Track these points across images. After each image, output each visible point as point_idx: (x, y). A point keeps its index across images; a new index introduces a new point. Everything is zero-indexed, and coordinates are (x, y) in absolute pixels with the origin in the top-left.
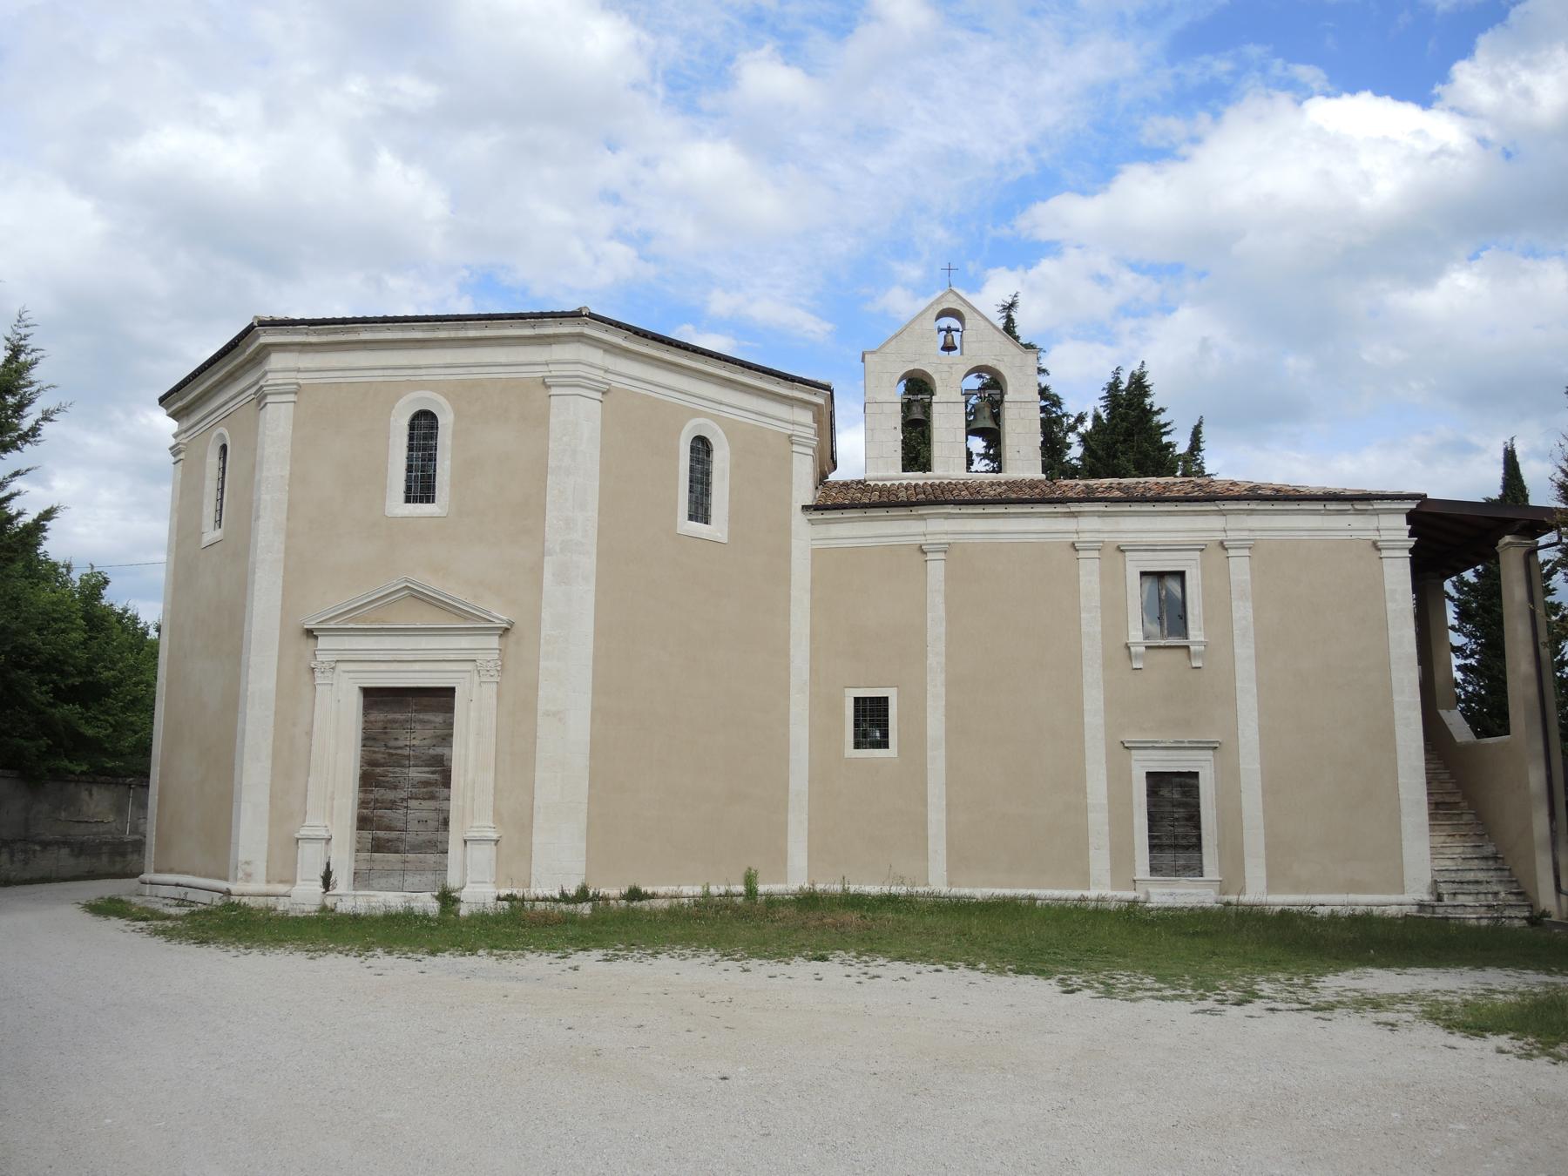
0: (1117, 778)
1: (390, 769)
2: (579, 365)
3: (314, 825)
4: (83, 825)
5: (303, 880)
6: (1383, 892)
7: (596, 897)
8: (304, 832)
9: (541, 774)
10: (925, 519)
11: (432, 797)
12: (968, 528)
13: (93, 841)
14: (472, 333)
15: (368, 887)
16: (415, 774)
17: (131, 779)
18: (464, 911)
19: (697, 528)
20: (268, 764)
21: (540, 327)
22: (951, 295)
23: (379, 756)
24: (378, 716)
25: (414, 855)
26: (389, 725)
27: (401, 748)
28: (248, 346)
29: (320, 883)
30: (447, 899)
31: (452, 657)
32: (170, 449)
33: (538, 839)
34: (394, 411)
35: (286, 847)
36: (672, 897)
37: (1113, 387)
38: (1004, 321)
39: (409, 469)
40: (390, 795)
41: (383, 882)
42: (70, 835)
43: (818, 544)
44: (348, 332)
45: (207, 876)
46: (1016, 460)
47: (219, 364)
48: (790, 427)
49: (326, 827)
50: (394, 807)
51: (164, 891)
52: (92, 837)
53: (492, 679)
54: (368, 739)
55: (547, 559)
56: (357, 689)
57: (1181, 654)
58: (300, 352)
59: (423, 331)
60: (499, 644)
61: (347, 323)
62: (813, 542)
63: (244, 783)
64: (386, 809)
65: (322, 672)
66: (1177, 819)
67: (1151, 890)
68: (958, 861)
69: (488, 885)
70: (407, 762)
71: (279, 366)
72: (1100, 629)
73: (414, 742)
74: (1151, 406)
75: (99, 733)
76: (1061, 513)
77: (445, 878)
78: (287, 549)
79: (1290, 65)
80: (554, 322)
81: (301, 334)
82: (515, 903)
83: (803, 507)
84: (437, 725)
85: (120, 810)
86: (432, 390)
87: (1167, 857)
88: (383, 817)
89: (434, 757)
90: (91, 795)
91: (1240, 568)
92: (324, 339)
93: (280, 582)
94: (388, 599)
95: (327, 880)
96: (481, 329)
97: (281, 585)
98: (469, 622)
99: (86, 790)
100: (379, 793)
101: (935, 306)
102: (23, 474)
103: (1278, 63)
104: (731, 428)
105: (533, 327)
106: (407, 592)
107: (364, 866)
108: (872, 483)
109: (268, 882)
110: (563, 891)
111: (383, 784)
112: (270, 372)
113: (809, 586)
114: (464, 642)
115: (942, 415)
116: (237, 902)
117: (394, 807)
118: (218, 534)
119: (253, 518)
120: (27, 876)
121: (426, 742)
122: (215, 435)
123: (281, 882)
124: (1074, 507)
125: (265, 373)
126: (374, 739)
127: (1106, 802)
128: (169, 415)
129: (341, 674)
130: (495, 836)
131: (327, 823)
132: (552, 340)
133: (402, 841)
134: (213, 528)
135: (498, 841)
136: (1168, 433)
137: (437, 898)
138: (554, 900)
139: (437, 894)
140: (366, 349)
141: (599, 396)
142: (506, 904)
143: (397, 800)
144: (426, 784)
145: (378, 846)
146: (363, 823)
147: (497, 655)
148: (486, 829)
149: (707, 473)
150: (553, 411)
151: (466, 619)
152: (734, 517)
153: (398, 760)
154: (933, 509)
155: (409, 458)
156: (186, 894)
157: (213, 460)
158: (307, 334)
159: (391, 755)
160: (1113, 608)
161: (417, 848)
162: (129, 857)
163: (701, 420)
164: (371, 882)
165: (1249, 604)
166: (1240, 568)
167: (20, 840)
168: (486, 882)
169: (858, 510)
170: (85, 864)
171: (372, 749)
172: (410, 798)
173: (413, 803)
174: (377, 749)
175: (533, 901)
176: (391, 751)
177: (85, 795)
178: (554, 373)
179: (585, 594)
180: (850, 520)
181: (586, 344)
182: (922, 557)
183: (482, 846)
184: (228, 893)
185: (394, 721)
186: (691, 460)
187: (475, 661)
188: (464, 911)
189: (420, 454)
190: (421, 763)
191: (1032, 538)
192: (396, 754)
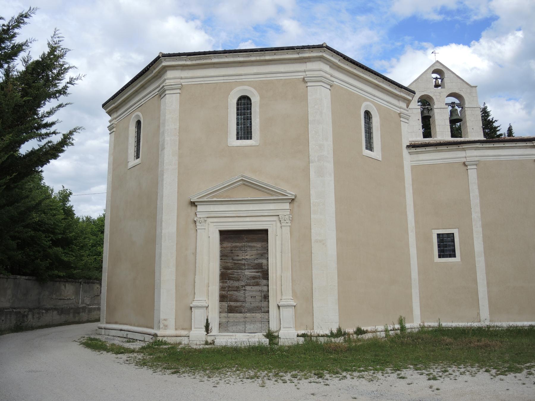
2: (321, 72)
3: (200, 299)
4: (62, 301)
7: (345, 334)
8: (194, 304)
10: (465, 150)
11: (258, 284)
13: (67, 307)
15: (227, 331)
16: (248, 273)
17: (81, 280)
20: (174, 269)
23: (229, 264)
24: (228, 245)
26: (233, 249)
28: (155, 69)
31: (266, 214)
32: (108, 127)
33: (316, 305)
34: (230, 96)
39: (238, 124)
40: (236, 284)
41: (234, 328)
42: (57, 305)
43: (414, 163)
44: (206, 59)
45: (139, 326)
46: (472, 132)
49: (205, 301)
50: (238, 290)
51: (113, 333)
52: (66, 306)
54: (223, 256)
55: (311, 164)
56: (218, 230)
58: (182, 70)
59: (243, 57)
60: (290, 207)
61: (206, 54)
62: (412, 163)
64: (234, 291)
65: (200, 223)
69: (292, 329)
70: (244, 267)
73: (247, 257)
74: (492, 119)
75: (69, 259)
76: (529, 146)
78: (179, 163)
79: (420, 43)
81: (183, 60)
84: (258, 248)
85: (77, 293)
86: (248, 86)
88: (233, 295)
90: (65, 287)
92: (194, 62)
94: (232, 186)
95: (207, 328)
96: (272, 55)
97: (177, 180)
99: (63, 285)
100: (230, 283)
101: (431, 68)
102: (63, 106)
103: (416, 42)
104: (379, 107)
106: (241, 182)
107: (224, 320)
109: (176, 329)
110: (331, 331)
112: (168, 79)
113: (411, 183)
114: (272, 206)
115: (438, 114)
116: (161, 340)
117: (238, 290)
119: (160, 149)
120: (39, 324)
121: (253, 257)
122: (134, 116)
123: (183, 329)
125: (165, 80)
126: (226, 256)
128: (106, 112)
129: (210, 223)
130: (295, 304)
131: (206, 299)
132: (307, 60)
133: (243, 307)
134: (134, 159)
136: (499, 130)
138: (327, 336)
139: (265, 334)
140: (214, 67)
141: (329, 87)
142: (301, 340)
143: (240, 286)
144: (254, 278)
145: (231, 310)
146: (223, 298)
148: (288, 300)
150: (309, 94)
151: (272, 195)
152: (383, 149)
153: (239, 266)
154: (470, 145)
155: (237, 119)
156: (127, 335)
158: (186, 60)
159: (235, 264)
161: (251, 310)
162: (81, 314)
163: (368, 103)
164: (228, 328)
167: (36, 308)
168: (291, 328)
169: (434, 147)
170: (63, 318)
173: (248, 288)
174: (228, 261)
175: (317, 337)
176: (235, 262)
177: (63, 287)
179: (330, 180)
181: (323, 62)
182: (465, 168)
183: (288, 309)
184: (155, 335)
185: (236, 247)
187: (278, 215)
189: (242, 116)
192: (238, 263)
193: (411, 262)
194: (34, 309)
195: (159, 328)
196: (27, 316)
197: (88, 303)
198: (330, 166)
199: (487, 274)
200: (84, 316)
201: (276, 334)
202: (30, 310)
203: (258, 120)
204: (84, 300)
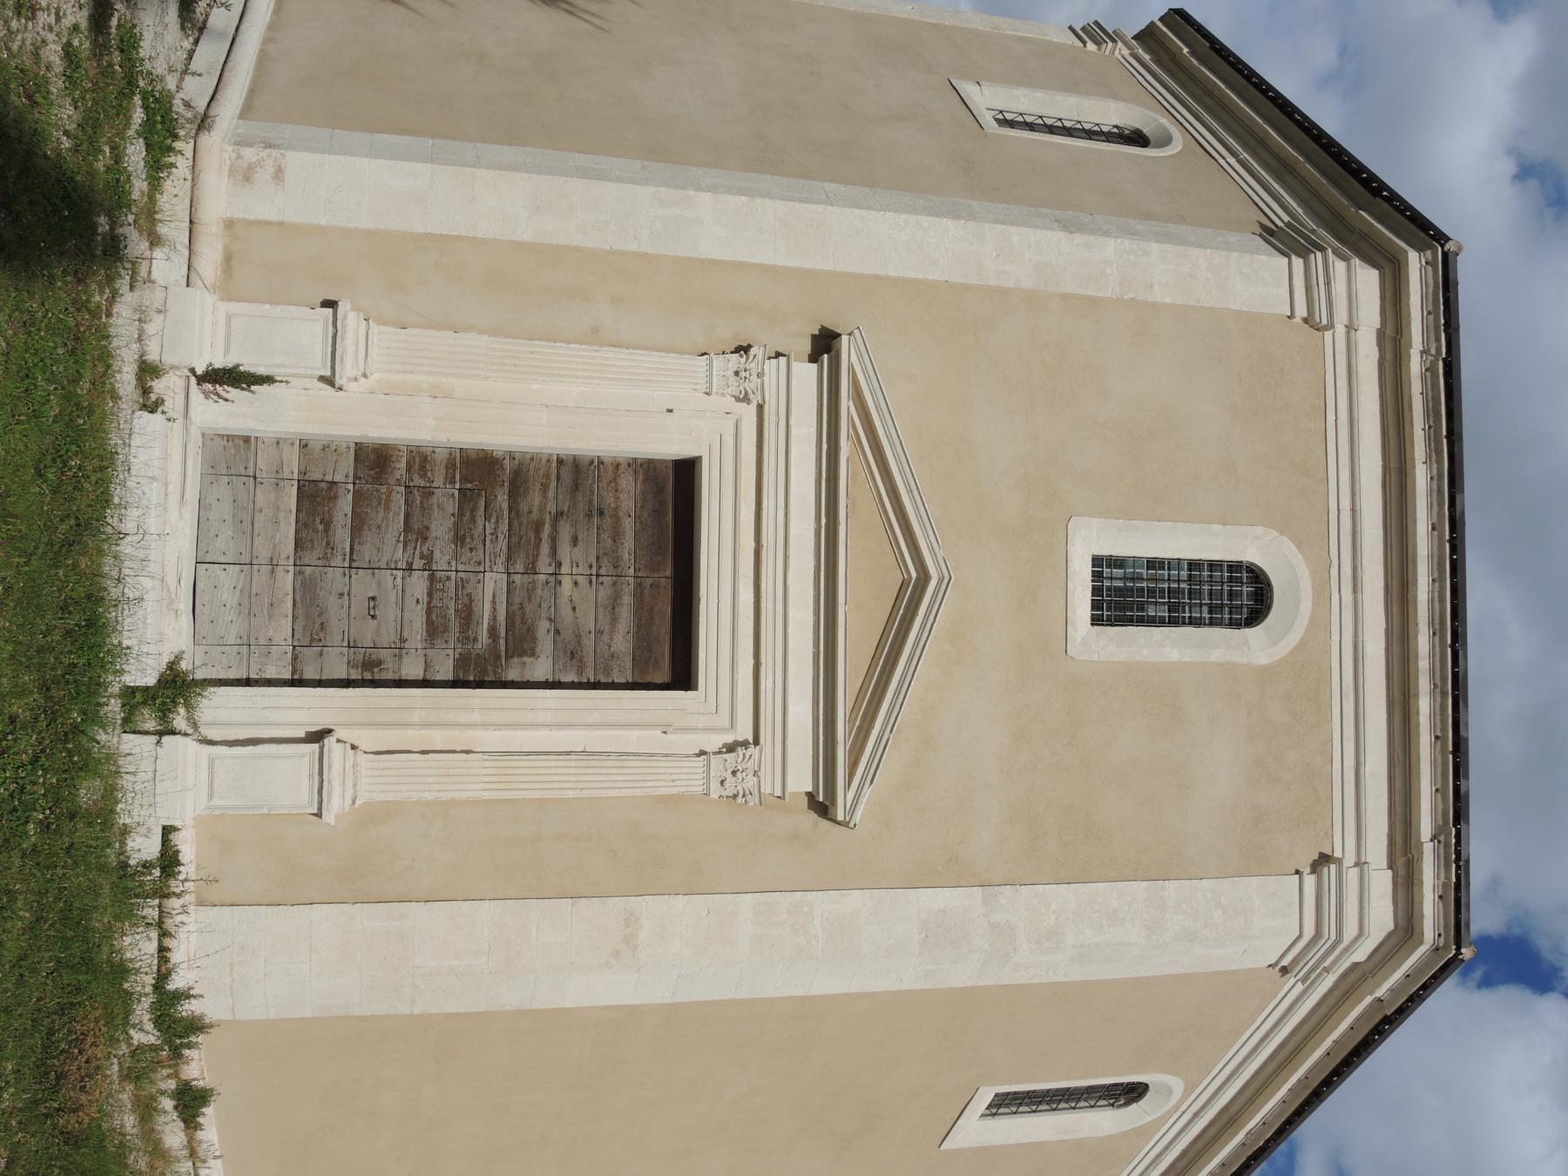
1: (504, 527)
5: (229, 318)
8: (351, 321)
14: (1424, 705)
16: (491, 589)
20: (524, 233)
21: (1436, 852)
23: (535, 498)
25: (290, 589)
26: (608, 520)
29: (219, 363)
31: (766, 683)
40: (441, 528)
41: (225, 509)
53: (715, 784)
60: (794, 795)
64: (407, 515)
65: (737, 373)
70: (519, 567)
73: (567, 583)
78: (1004, 292)
80: (1445, 886)
81: (1426, 340)
82: (157, 872)
84: (606, 637)
88: (387, 508)
93: (934, 275)
100: (446, 499)
107: (264, 462)
111: (467, 508)
116: (178, 145)
118: (988, 120)
121: (566, 612)
123: (228, 258)
126: (576, 487)
133: (325, 557)
138: (163, 977)
144: (467, 615)
147: (769, 791)
148: (349, 784)
150: (1271, 882)
157: (1112, 114)
159: (538, 527)
164: (226, 479)
168: (211, 797)
171: (553, 484)
172: (432, 578)
173: (418, 584)
174: (551, 493)
175: (160, 924)
184: (204, 122)
185: (617, 535)
190: (517, 600)
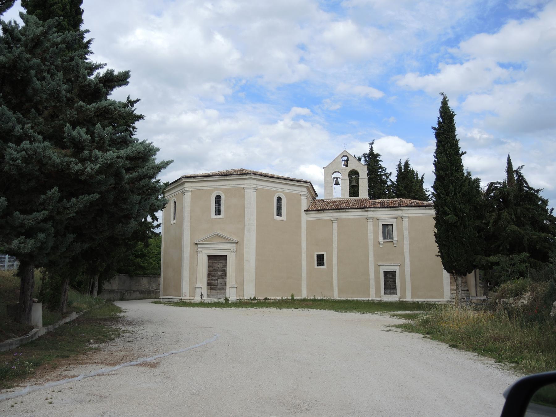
0: (377, 272)
1: (214, 273)
3: (199, 284)
4: (141, 287)
6: (439, 298)
7: (257, 299)
8: (197, 286)
9: (245, 273)
11: (223, 278)
12: (342, 215)
15: (210, 298)
16: (219, 273)
18: (230, 302)
19: (279, 218)
22: (345, 152)
23: (211, 270)
24: (211, 261)
27: (216, 268)
28: (180, 181)
30: (227, 300)
33: (245, 287)
35: (193, 290)
36: (274, 300)
37: (400, 165)
38: (370, 147)
40: (214, 278)
43: (309, 219)
47: (174, 183)
48: (301, 192)
54: (209, 266)
56: (206, 256)
57: (392, 243)
63: (184, 276)
66: (391, 282)
67: (384, 298)
68: (340, 291)
71: (187, 186)
72: (372, 238)
73: (219, 267)
77: (226, 296)
78: (191, 226)
83: (304, 211)
87: (389, 290)
89: (223, 270)
90: (143, 279)
91: (405, 223)
92: (196, 180)
95: (202, 296)
98: (228, 241)
100: (212, 278)
104: (286, 194)
105: (241, 176)
107: (209, 293)
108: (325, 200)
109: (189, 297)
114: (228, 245)
120: (131, 298)
121: (221, 267)
122: (173, 199)
123: (192, 297)
124: (366, 210)
125: (184, 188)
127: (374, 278)
130: (236, 287)
135: (236, 288)
137: (224, 300)
138: (249, 300)
144: (221, 276)
145: (212, 289)
149: (281, 205)
153: (215, 271)
155: (216, 206)
156: (171, 300)
160: (376, 233)
161: (220, 289)
162: (151, 294)
163: (279, 193)
165: (408, 231)
166: (405, 223)
173: (219, 280)
178: (246, 186)
180: (315, 213)
182: (331, 222)
184: (181, 299)
185: (215, 262)
186: (277, 202)
188: (230, 302)
191: (357, 217)
193: (302, 268)
194: (128, 290)
195: (183, 296)
196: (125, 294)
197: (155, 288)
198: (254, 227)
199: (338, 274)
200: (153, 295)
201: (228, 299)
202: (126, 291)
203: (224, 207)
204: (153, 286)
